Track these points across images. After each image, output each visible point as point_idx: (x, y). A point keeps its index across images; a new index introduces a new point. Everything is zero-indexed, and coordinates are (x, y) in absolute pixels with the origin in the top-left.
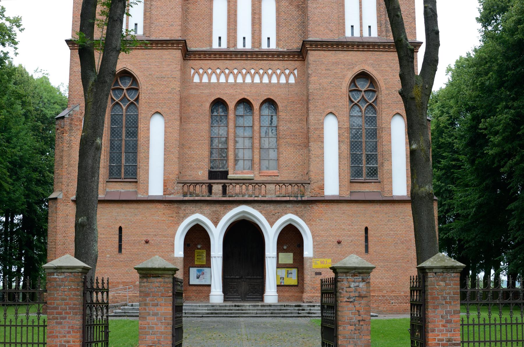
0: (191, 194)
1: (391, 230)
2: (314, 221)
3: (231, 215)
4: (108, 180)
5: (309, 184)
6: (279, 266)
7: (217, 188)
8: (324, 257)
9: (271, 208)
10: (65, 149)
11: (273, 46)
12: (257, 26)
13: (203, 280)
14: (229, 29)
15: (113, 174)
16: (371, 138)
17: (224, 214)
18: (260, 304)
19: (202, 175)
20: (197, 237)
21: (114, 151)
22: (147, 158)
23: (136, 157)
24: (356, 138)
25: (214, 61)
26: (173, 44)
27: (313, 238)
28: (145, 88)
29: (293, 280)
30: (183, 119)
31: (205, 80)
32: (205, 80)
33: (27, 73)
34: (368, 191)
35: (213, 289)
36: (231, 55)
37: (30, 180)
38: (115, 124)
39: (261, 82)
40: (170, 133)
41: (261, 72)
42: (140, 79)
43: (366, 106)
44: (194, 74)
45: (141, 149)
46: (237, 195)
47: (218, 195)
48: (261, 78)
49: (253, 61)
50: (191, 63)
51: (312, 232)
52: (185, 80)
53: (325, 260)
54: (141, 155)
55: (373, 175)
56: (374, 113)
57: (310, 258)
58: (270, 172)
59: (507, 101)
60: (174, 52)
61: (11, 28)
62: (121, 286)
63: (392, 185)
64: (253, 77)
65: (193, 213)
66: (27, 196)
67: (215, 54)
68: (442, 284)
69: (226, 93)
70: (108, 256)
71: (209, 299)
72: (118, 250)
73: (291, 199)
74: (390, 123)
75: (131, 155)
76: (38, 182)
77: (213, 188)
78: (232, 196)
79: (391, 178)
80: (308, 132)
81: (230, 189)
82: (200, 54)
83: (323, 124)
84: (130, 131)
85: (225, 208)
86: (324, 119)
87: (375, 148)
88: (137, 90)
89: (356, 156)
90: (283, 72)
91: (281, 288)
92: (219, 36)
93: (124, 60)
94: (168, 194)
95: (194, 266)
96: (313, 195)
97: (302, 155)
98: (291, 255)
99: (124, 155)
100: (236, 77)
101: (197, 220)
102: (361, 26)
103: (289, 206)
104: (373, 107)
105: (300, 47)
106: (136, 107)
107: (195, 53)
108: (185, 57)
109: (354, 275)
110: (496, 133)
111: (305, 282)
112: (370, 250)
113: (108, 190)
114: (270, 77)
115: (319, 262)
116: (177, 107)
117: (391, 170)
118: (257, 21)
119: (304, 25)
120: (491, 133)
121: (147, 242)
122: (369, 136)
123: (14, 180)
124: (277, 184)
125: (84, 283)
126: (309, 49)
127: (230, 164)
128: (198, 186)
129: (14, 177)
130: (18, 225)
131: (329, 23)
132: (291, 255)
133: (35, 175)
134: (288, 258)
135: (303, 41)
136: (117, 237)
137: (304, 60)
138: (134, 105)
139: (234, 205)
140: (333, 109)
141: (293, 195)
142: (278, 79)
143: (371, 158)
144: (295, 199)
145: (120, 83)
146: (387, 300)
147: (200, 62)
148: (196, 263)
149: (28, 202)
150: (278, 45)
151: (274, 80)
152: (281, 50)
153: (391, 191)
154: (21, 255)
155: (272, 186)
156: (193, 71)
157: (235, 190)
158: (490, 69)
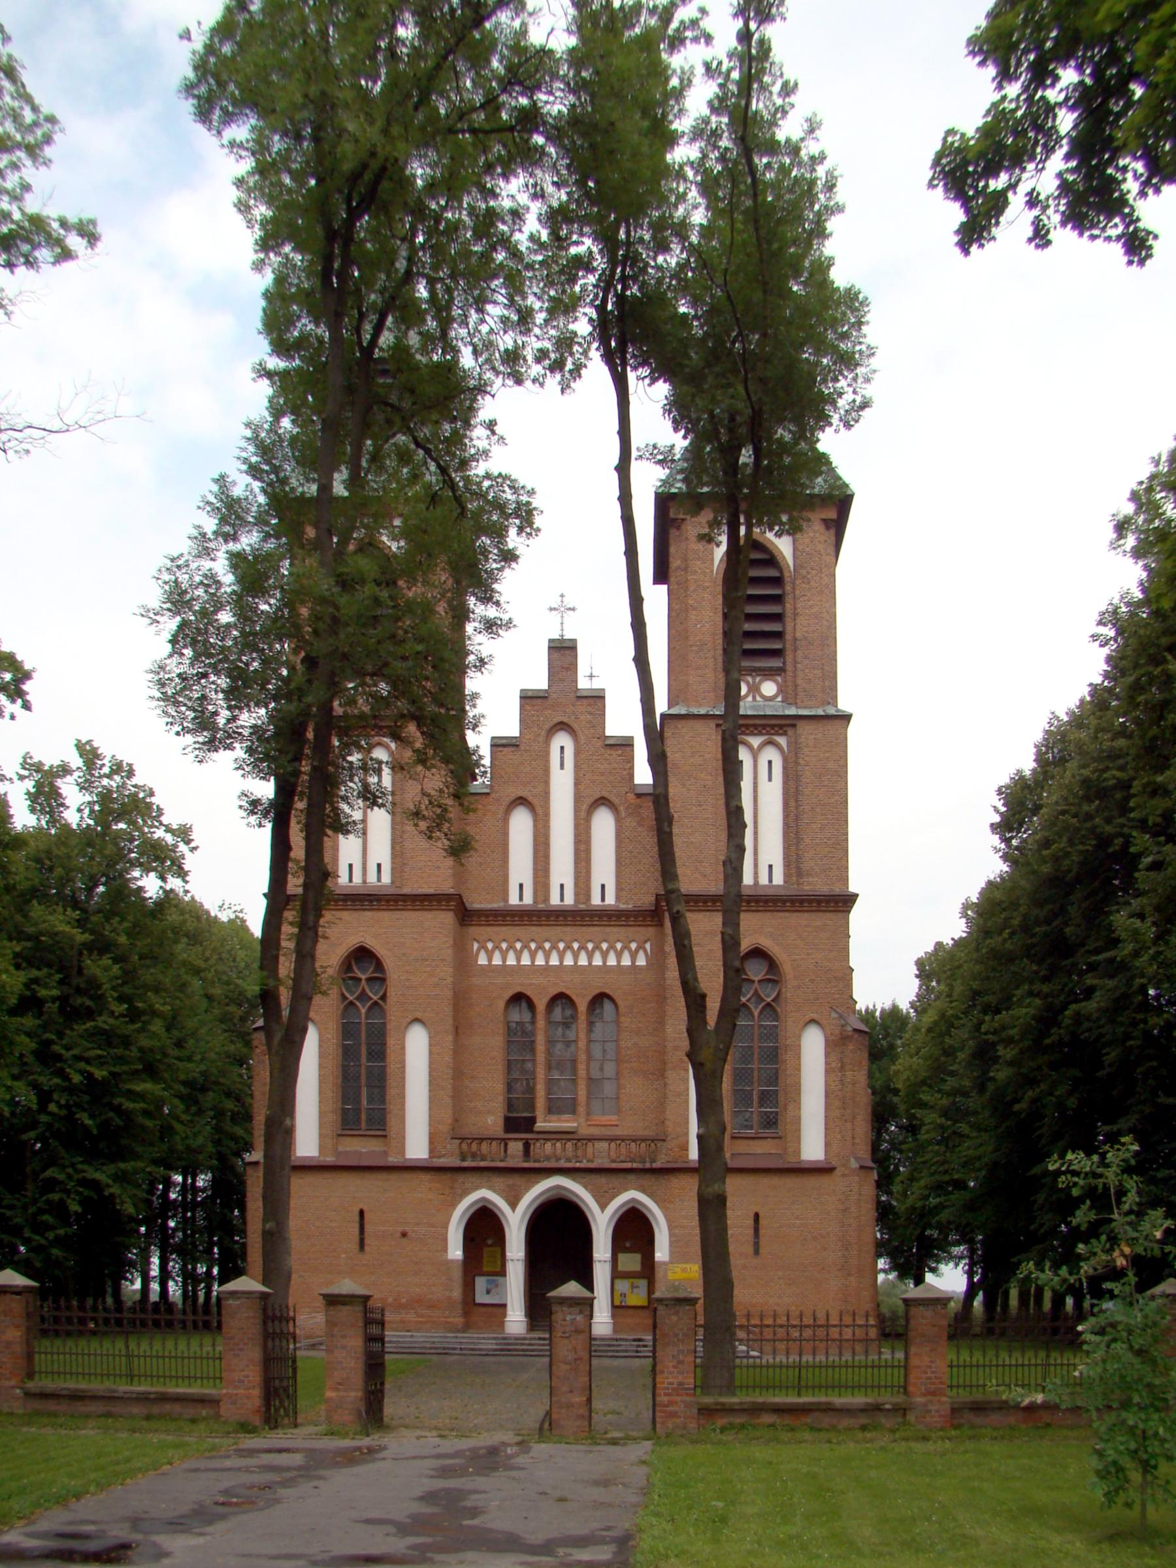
0: (474, 1156)
8: (687, 1262)
9: (601, 1180)
11: (610, 900)
12: (583, 855)
14: (536, 870)
17: (527, 1189)
19: (493, 1122)
20: (484, 1229)
26: (439, 901)
27: (670, 1229)
32: (497, 960)
33: (208, 912)
35: (509, 1312)
37: (220, 1114)
44: (479, 950)
45: (391, 1082)
46: (548, 1158)
50: (474, 931)
52: (463, 961)
53: (688, 1266)
54: (391, 1092)
57: (664, 1263)
58: (605, 1120)
59: (1032, 982)
61: (175, 846)
64: (576, 957)
65: (477, 1188)
66: (218, 1143)
67: (513, 916)
68: (674, 1318)
72: (357, 1247)
73: (635, 1165)
75: (376, 1090)
76: (235, 1118)
81: (536, 1149)
82: (487, 916)
87: (774, 1078)
88: (383, 980)
91: (621, 1311)
95: (482, 1274)
99: (364, 1091)
101: (483, 1199)
103: (631, 1177)
104: (775, 1010)
106: (383, 1010)
109: (571, 1306)
110: (1009, 1041)
113: (341, 1149)
114: (605, 956)
116: (448, 1010)
117: (799, 1118)
118: (583, 855)
120: (1002, 1041)
123: (194, 1115)
125: (265, 1310)
129: (194, 1109)
130: (204, 1190)
133: (229, 1105)
134: (631, 1262)
136: (357, 1225)
138: (377, 1007)
143: (767, 1098)
144: (640, 1166)
147: (489, 929)
149: (219, 1152)
150: (618, 898)
151: (612, 961)
152: (623, 906)
153: (798, 1152)
154: (212, 1244)
155: (604, 1145)
157: (545, 1150)
158: (1005, 925)
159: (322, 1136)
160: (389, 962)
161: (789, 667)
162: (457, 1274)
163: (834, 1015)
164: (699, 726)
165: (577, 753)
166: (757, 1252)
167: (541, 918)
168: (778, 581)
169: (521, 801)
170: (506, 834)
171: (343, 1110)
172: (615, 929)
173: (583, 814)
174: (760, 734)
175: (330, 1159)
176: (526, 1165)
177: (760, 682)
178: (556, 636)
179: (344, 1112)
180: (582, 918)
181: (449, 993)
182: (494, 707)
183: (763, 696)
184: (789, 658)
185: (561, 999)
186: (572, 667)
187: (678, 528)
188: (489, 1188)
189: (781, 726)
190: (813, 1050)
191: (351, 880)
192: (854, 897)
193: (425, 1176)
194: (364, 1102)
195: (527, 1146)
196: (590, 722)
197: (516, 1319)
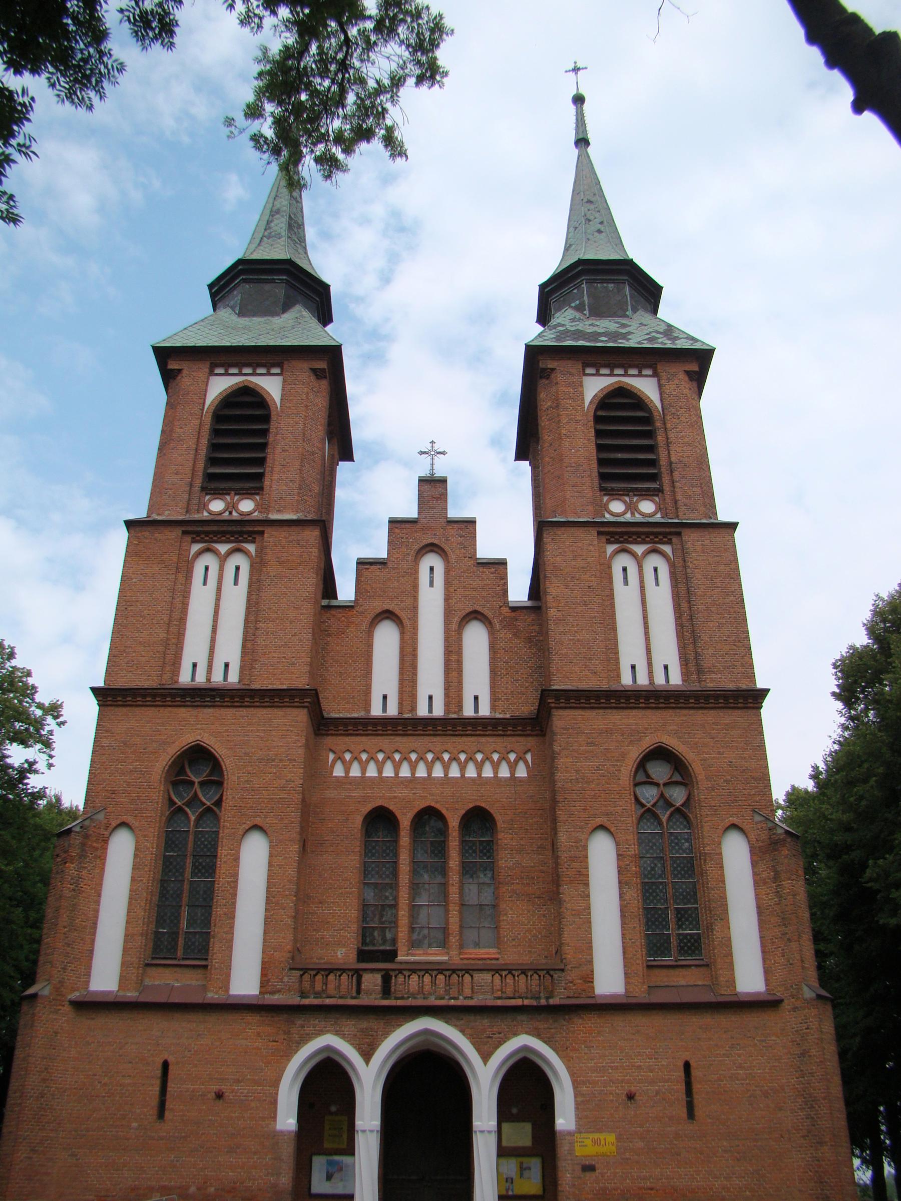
1: (740, 1067)
3: (397, 1038)
4: (150, 961)
5: (563, 970)
6: (503, 1152)
8: (599, 1131)
9: (483, 1023)
10: (67, 893)
11: (485, 711)
12: (454, 674)
13: (340, 1184)
14: (402, 681)
16: (683, 877)
17: (386, 1034)
19: (344, 953)
20: (327, 1087)
21: (167, 903)
23: (210, 914)
24: (653, 876)
25: (373, 737)
26: (292, 697)
27: (575, 1087)
28: (235, 778)
29: (532, 1185)
31: (355, 771)
34: (683, 983)
39: (463, 775)
40: (280, 866)
41: (463, 757)
42: (227, 762)
43: (668, 813)
44: (334, 762)
47: (373, 996)
48: (463, 768)
49: (448, 738)
50: (329, 741)
51: (572, 1075)
52: (314, 771)
53: (602, 1136)
54: (218, 911)
55: (693, 952)
56: (685, 827)
57: (570, 1133)
60: (295, 712)
63: (733, 970)
65: (320, 1033)
69: (395, 797)
70: (135, 1125)
72: (155, 1112)
73: (527, 1002)
74: (720, 843)
75: (199, 911)
77: (363, 979)
78: (402, 998)
79: (731, 954)
80: (557, 864)
82: (346, 725)
83: (585, 848)
84: (200, 864)
86: (587, 839)
87: (692, 896)
88: (220, 784)
90: (503, 758)
92: (383, 693)
93: (199, 726)
94: (270, 993)
95: (319, 1153)
96: (571, 995)
97: (544, 916)
98: (528, 1127)
101: (328, 1048)
102: (650, 664)
104: (685, 817)
105: (536, 711)
106: (217, 818)
108: (319, 730)
111: (560, 1188)
112: (699, 1112)
113: (147, 982)
115: (588, 1142)
116: (294, 815)
117: (729, 939)
118: (454, 665)
119: (542, 668)
121: (219, 1096)
122: (679, 872)
124: (497, 971)
126: (553, 705)
127: (400, 935)
128: (331, 977)
131: (590, 659)
132: (528, 1127)
135: (543, 691)
136: (158, 1082)
137: (544, 735)
138: (211, 813)
140: (605, 820)
141: (529, 996)
142: (494, 770)
144: (534, 1003)
145: (188, 770)
147: (347, 739)
148: (327, 1145)
150: (493, 708)
151: (488, 772)
153: (732, 982)
155: (487, 977)
156: (331, 756)
157: (410, 988)
159: (124, 964)
160: (228, 762)
161: (667, 487)
162: (288, 1151)
163: (757, 818)
164: (579, 532)
165: (447, 572)
166: (691, 1115)
167: (406, 727)
168: (648, 420)
169: (388, 615)
170: (370, 646)
171: (156, 933)
172: (491, 740)
173: (454, 626)
174: (644, 542)
175: (131, 995)
176: (386, 1002)
177: (637, 502)
180: (453, 727)
181: (298, 797)
182: (360, 532)
183: (641, 513)
184: (666, 480)
185: (428, 817)
186: (443, 497)
187: (548, 377)
188: (337, 1033)
189: (665, 535)
190: (736, 857)
191: (193, 679)
192: (764, 692)
193: (253, 1019)
194: (184, 924)
195: (387, 979)
196: (461, 543)
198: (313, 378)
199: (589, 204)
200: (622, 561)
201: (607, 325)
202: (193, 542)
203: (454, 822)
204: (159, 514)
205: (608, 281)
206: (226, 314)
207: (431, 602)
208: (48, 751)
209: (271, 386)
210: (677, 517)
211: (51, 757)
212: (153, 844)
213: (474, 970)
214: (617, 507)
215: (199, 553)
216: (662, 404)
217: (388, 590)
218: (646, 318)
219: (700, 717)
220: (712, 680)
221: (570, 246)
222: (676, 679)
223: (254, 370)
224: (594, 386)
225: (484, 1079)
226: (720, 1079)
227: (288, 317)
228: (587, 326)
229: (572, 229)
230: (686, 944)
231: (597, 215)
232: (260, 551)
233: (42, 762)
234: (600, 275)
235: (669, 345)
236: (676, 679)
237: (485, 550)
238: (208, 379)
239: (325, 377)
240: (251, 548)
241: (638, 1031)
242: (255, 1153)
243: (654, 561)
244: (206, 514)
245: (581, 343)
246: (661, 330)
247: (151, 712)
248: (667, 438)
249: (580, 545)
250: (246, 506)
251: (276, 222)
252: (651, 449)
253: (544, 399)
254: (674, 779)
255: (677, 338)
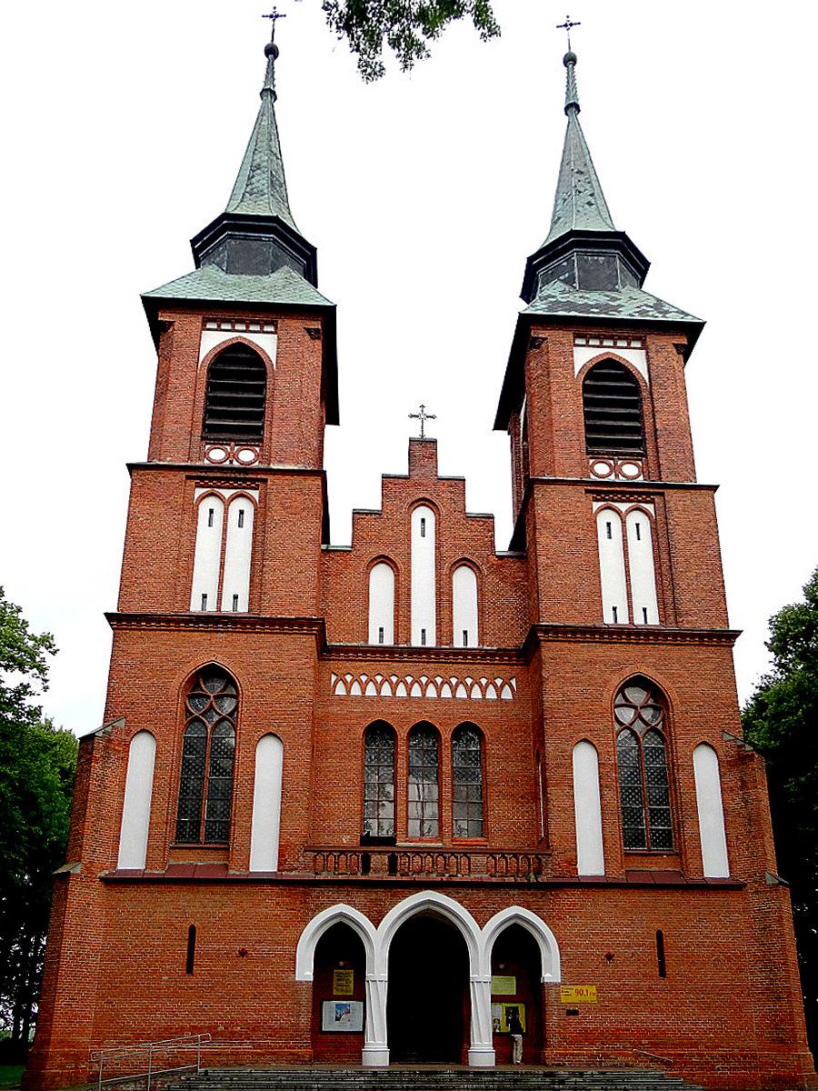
2: (560, 918)
4: (173, 845)
5: (550, 855)
7: (379, 860)
11: (473, 643)
15: (184, 836)
18: (461, 1068)
20: (341, 949)
22: (248, 832)
26: (301, 625)
30: (318, 750)
31: (356, 690)
35: (369, 1040)
36: (401, 654)
38: (191, 753)
39: (454, 696)
44: (336, 682)
52: (322, 691)
53: (584, 988)
54: (238, 803)
62: (188, 1036)
71: (360, 1057)
81: (401, 861)
85: (394, 895)
89: (632, 811)
94: (287, 871)
100: (411, 689)
102: (630, 607)
107: (338, 650)
112: (669, 971)
113: (172, 862)
114: (469, 690)
121: (243, 953)
139: (406, 891)
142: (490, 692)
146: (707, 1063)
150: (481, 641)
155: (482, 859)
161: (650, 452)
162: (306, 997)
165: (438, 523)
166: (663, 973)
167: (400, 654)
168: (636, 390)
169: (384, 559)
171: (179, 822)
173: (445, 571)
175: (158, 872)
176: (393, 878)
178: (417, 435)
179: (180, 825)
180: (443, 656)
185: (424, 730)
186: (433, 456)
187: (538, 347)
189: (648, 494)
190: (705, 769)
192: (737, 633)
193: (268, 889)
197: (377, 1050)
198: (307, 337)
199: (577, 171)
200: (606, 517)
201: (595, 298)
202: (196, 487)
203: (446, 735)
204: (160, 460)
205: (599, 255)
206: (210, 270)
207: (423, 552)
208: (41, 676)
209: (265, 342)
210: (660, 479)
211: (46, 681)
212: (174, 751)
213: (470, 853)
214: (601, 469)
215: (203, 497)
216: (650, 376)
217: (381, 537)
218: (635, 293)
219: (674, 652)
220: (688, 622)
221: (559, 218)
222: (654, 620)
223: (262, 327)
224: (584, 356)
225: (481, 941)
226: (688, 946)
227: (277, 277)
228: (576, 298)
229: (560, 201)
230: (658, 838)
231: (588, 186)
232: (264, 498)
233: (36, 685)
234: (588, 251)
235: (660, 318)
236: (654, 620)
237: (474, 505)
238: (201, 333)
239: (319, 338)
240: (255, 494)
241: (616, 906)
242: (276, 999)
243: (636, 517)
244: (206, 462)
245: (573, 313)
246: (652, 305)
247: (165, 636)
248: (653, 407)
249: (569, 501)
250: (246, 456)
251: (257, 178)
252: (638, 417)
253: (534, 366)
254: (649, 702)
255: (668, 312)
